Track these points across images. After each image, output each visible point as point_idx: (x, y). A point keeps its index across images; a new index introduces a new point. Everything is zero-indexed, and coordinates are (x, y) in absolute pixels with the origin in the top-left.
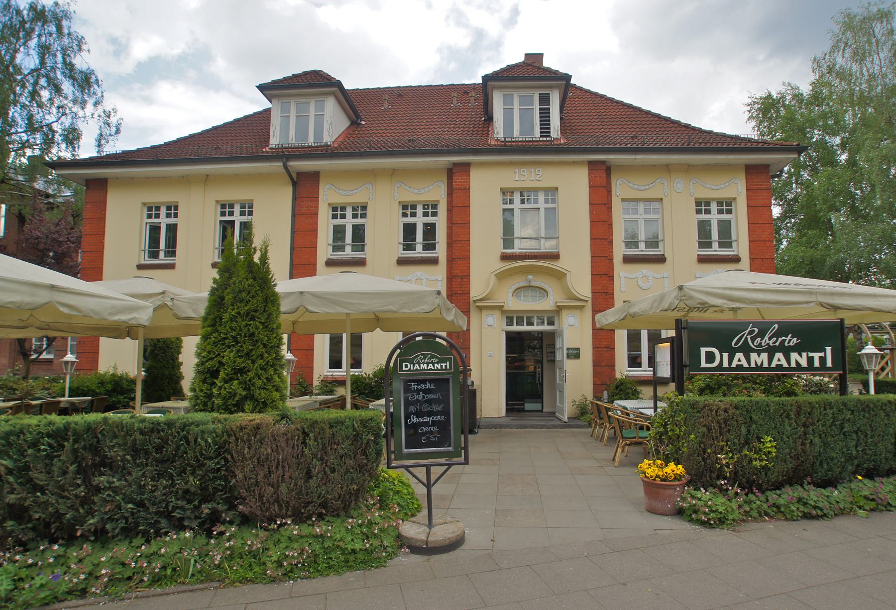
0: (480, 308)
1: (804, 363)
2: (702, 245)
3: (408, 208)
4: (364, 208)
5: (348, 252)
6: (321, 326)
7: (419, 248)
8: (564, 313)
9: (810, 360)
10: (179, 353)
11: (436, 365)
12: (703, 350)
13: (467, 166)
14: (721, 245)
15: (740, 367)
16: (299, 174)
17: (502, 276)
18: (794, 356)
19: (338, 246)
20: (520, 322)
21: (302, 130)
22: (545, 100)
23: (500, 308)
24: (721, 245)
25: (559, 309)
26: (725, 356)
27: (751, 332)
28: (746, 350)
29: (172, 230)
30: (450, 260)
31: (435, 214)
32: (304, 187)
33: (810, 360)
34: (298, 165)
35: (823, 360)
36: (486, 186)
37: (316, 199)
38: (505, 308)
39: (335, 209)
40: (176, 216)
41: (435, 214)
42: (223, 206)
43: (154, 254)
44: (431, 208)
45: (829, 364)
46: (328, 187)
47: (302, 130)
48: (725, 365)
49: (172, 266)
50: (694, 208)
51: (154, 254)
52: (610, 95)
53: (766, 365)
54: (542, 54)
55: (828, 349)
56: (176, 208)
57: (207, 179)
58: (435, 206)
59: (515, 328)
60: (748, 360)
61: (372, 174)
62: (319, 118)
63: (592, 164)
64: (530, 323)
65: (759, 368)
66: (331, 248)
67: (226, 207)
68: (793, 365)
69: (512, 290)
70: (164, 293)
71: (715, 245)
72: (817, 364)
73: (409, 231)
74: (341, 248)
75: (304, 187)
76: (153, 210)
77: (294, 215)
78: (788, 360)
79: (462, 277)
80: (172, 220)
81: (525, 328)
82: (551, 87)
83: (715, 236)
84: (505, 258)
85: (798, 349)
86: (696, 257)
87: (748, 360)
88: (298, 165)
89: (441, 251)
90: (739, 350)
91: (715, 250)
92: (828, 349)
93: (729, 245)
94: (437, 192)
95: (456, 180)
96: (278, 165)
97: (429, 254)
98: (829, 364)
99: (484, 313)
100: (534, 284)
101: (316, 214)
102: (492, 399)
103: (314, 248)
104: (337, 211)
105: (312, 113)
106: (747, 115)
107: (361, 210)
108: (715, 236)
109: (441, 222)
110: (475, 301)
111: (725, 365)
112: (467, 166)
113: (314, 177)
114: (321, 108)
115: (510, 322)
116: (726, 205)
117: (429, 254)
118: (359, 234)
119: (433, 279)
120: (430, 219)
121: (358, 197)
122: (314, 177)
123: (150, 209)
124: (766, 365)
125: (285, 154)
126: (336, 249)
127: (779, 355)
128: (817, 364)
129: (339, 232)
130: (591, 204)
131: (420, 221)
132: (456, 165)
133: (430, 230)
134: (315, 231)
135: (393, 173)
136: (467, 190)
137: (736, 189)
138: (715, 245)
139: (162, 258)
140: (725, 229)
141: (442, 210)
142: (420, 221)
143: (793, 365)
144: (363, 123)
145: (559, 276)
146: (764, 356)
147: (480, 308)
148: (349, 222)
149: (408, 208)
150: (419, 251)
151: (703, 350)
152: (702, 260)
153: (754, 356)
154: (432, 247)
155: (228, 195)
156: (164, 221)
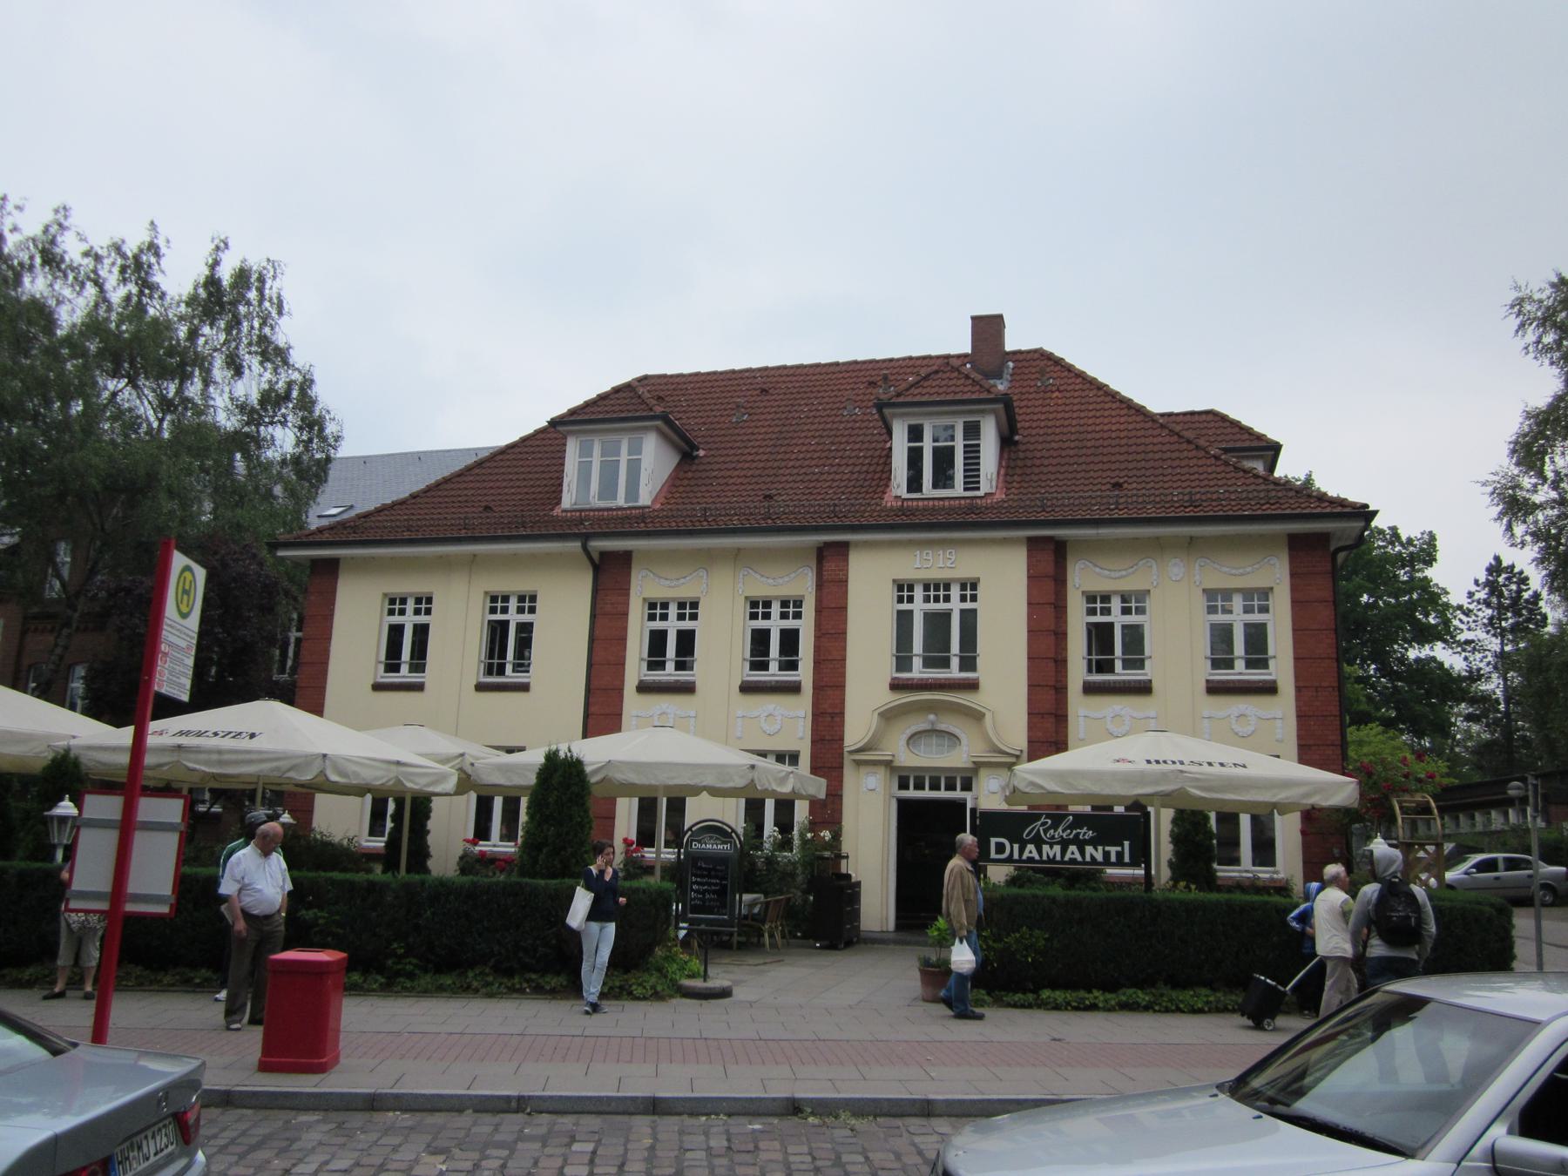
0: (859, 763)
1: (1099, 857)
2: (1216, 664)
3: (759, 608)
4: (695, 605)
5: (670, 673)
6: (628, 789)
7: (774, 667)
8: (983, 773)
9: (1107, 855)
10: (428, 817)
11: (1089, 849)
12: (993, 840)
13: (845, 546)
14: (1250, 664)
15: (1031, 860)
16: (604, 555)
17: (889, 716)
18: (1089, 849)
19: (656, 664)
20: (919, 786)
21: (608, 488)
22: (972, 431)
23: (888, 764)
24: (1250, 664)
25: (978, 766)
26: (1016, 847)
27: (1044, 824)
28: (1038, 842)
29: (422, 632)
30: (818, 688)
31: (798, 616)
32: (610, 575)
33: (1107, 855)
34: (598, 545)
35: (1120, 855)
36: (872, 579)
37: (625, 592)
38: (896, 764)
39: (652, 606)
40: (428, 612)
41: (798, 616)
42: (494, 599)
43: (393, 667)
44: (791, 606)
45: (1127, 859)
46: (644, 573)
47: (608, 488)
48: (1016, 856)
49: (419, 687)
50: (700, 611)
51: (393, 667)
52: (1114, 386)
53: (1058, 858)
54: (1000, 317)
55: (1126, 843)
56: (429, 600)
57: (473, 562)
58: (798, 603)
59: (912, 793)
60: (1040, 852)
61: (709, 559)
62: (634, 469)
63: (1032, 543)
64: (935, 786)
65: (1052, 860)
66: (645, 665)
67: (497, 601)
68: (1088, 858)
69: (905, 737)
70: (462, 755)
71: (1240, 665)
72: (1113, 858)
73: (760, 640)
74: (660, 665)
75: (610, 575)
76: (395, 603)
77: (593, 616)
78: (1082, 853)
79: (833, 715)
80: (422, 619)
81: (927, 794)
82: (982, 412)
83: (1239, 648)
84: (896, 686)
85: (1094, 843)
86: (1203, 685)
87: (1040, 852)
88: (598, 545)
89: (805, 673)
90: (1030, 842)
91: (1240, 672)
92: (1126, 843)
93: (1263, 663)
94: (802, 583)
95: (830, 564)
96: (575, 546)
97: (788, 676)
98: (1127, 859)
99: (864, 770)
100: (943, 727)
101: (626, 614)
102: (878, 904)
103: (621, 664)
104: (656, 609)
105: (624, 458)
106: (1514, 322)
107: (689, 608)
108: (1239, 648)
109: (806, 628)
110: (851, 752)
111: (1016, 856)
112: (845, 546)
113: (624, 561)
114: (636, 449)
115: (903, 785)
116: (1259, 597)
117: (788, 676)
118: (686, 641)
119: (790, 722)
120: (790, 624)
121: (686, 592)
122: (625, 559)
123: (392, 601)
124: (1058, 858)
125: (583, 527)
126: (653, 666)
127: (1073, 848)
128: (1113, 858)
129: (657, 640)
130: (1029, 604)
131: (775, 625)
132: (828, 545)
133: (790, 640)
134: (622, 640)
135: (737, 555)
136: (843, 583)
137: (1275, 573)
138: (1240, 665)
139: (405, 674)
140: (1257, 638)
141: (809, 610)
142: (775, 625)
143: (1088, 858)
144: (702, 453)
145: (977, 716)
146: (1057, 848)
147: (859, 763)
148: (672, 626)
149: (759, 608)
150: (774, 673)
151: (993, 840)
152: (1214, 689)
153: (1046, 848)
154: (793, 666)
155: (500, 585)
156: (409, 620)
